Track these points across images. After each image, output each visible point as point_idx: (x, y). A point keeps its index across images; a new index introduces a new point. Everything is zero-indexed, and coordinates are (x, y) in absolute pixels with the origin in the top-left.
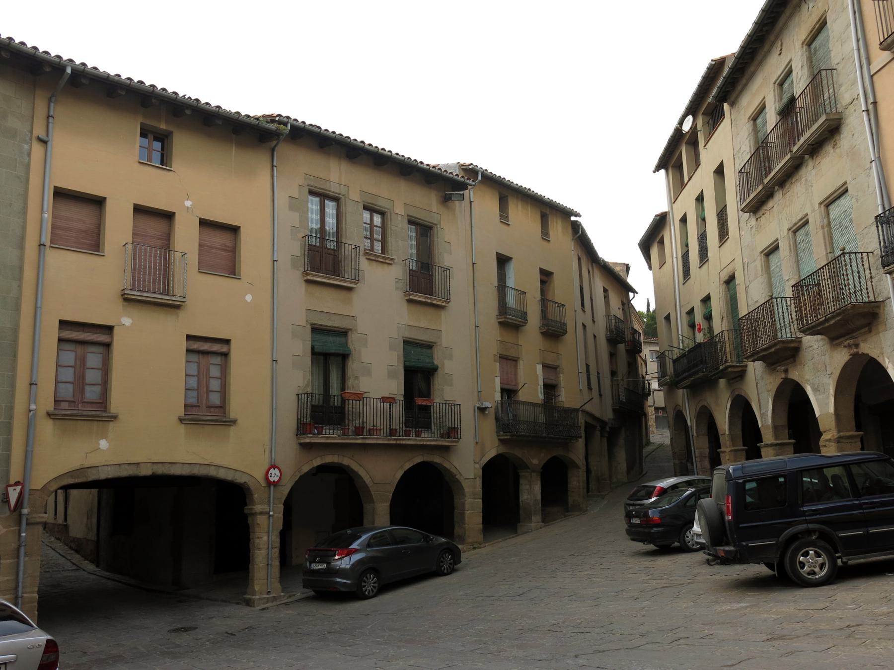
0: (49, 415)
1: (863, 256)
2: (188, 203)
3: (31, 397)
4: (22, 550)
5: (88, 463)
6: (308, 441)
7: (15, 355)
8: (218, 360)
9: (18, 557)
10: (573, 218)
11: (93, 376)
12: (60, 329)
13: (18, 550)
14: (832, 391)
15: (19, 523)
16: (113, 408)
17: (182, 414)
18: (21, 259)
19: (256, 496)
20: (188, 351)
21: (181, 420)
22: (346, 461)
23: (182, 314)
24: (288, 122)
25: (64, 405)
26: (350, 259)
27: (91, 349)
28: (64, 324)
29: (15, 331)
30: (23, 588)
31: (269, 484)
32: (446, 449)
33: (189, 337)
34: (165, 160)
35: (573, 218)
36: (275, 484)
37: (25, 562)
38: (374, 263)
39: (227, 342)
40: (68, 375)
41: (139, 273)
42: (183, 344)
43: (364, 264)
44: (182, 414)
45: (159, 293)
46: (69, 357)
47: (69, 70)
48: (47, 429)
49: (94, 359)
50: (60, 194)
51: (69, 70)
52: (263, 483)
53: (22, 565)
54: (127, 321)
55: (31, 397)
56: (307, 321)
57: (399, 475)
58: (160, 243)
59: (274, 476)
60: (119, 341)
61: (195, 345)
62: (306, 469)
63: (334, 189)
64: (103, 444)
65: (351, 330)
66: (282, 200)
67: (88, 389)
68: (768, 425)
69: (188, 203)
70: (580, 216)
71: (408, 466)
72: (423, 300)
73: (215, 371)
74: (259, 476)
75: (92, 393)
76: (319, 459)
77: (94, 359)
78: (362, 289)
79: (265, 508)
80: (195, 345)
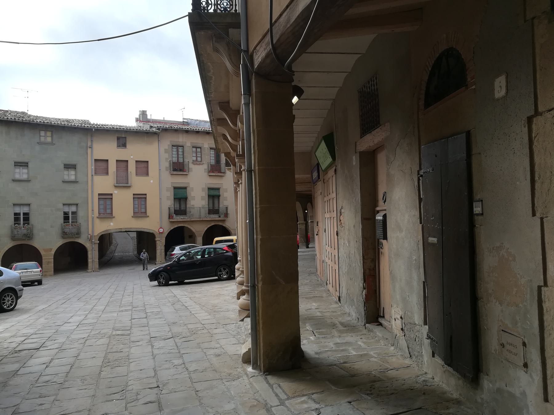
0: (97, 217)
1: (544, 110)
2: (132, 157)
3: (93, 214)
4: (93, 249)
5: (108, 229)
6: (171, 221)
7: (88, 204)
8: (144, 200)
9: (92, 251)
11: (108, 207)
12: (99, 195)
13: (92, 250)
15: (92, 244)
16: (114, 215)
17: (133, 216)
18: (88, 179)
19: (156, 236)
21: (132, 217)
22: (186, 225)
23: (131, 188)
24: (160, 128)
25: (102, 215)
26: (187, 165)
27: (108, 200)
28: (99, 194)
29: (88, 198)
30: (94, 258)
31: (160, 233)
32: (224, 221)
33: (134, 194)
34: (124, 145)
36: (162, 233)
37: (94, 253)
38: (196, 165)
40: (102, 207)
41: (119, 178)
42: (132, 196)
43: (191, 166)
44: (133, 216)
45: (118, 184)
46: (102, 202)
47: (94, 130)
48: (97, 221)
49: (108, 202)
50: (95, 160)
51: (94, 130)
52: (158, 233)
53: (93, 253)
54: (116, 192)
55: (93, 214)
56: (171, 186)
57: (206, 229)
58: (125, 169)
59: (161, 230)
60: (114, 197)
61: (101, 197)
62: (172, 228)
63: (181, 144)
64: (112, 224)
65: (187, 187)
66: (162, 150)
67: (107, 210)
69: (132, 157)
71: (209, 226)
72: (215, 175)
73: (143, 203)
74: (157, 231)
75: (109, 211)
76: (176, 225)
77: (108, 202)
78: (191, 174)
79: (159, 239)
80: (101, 197)
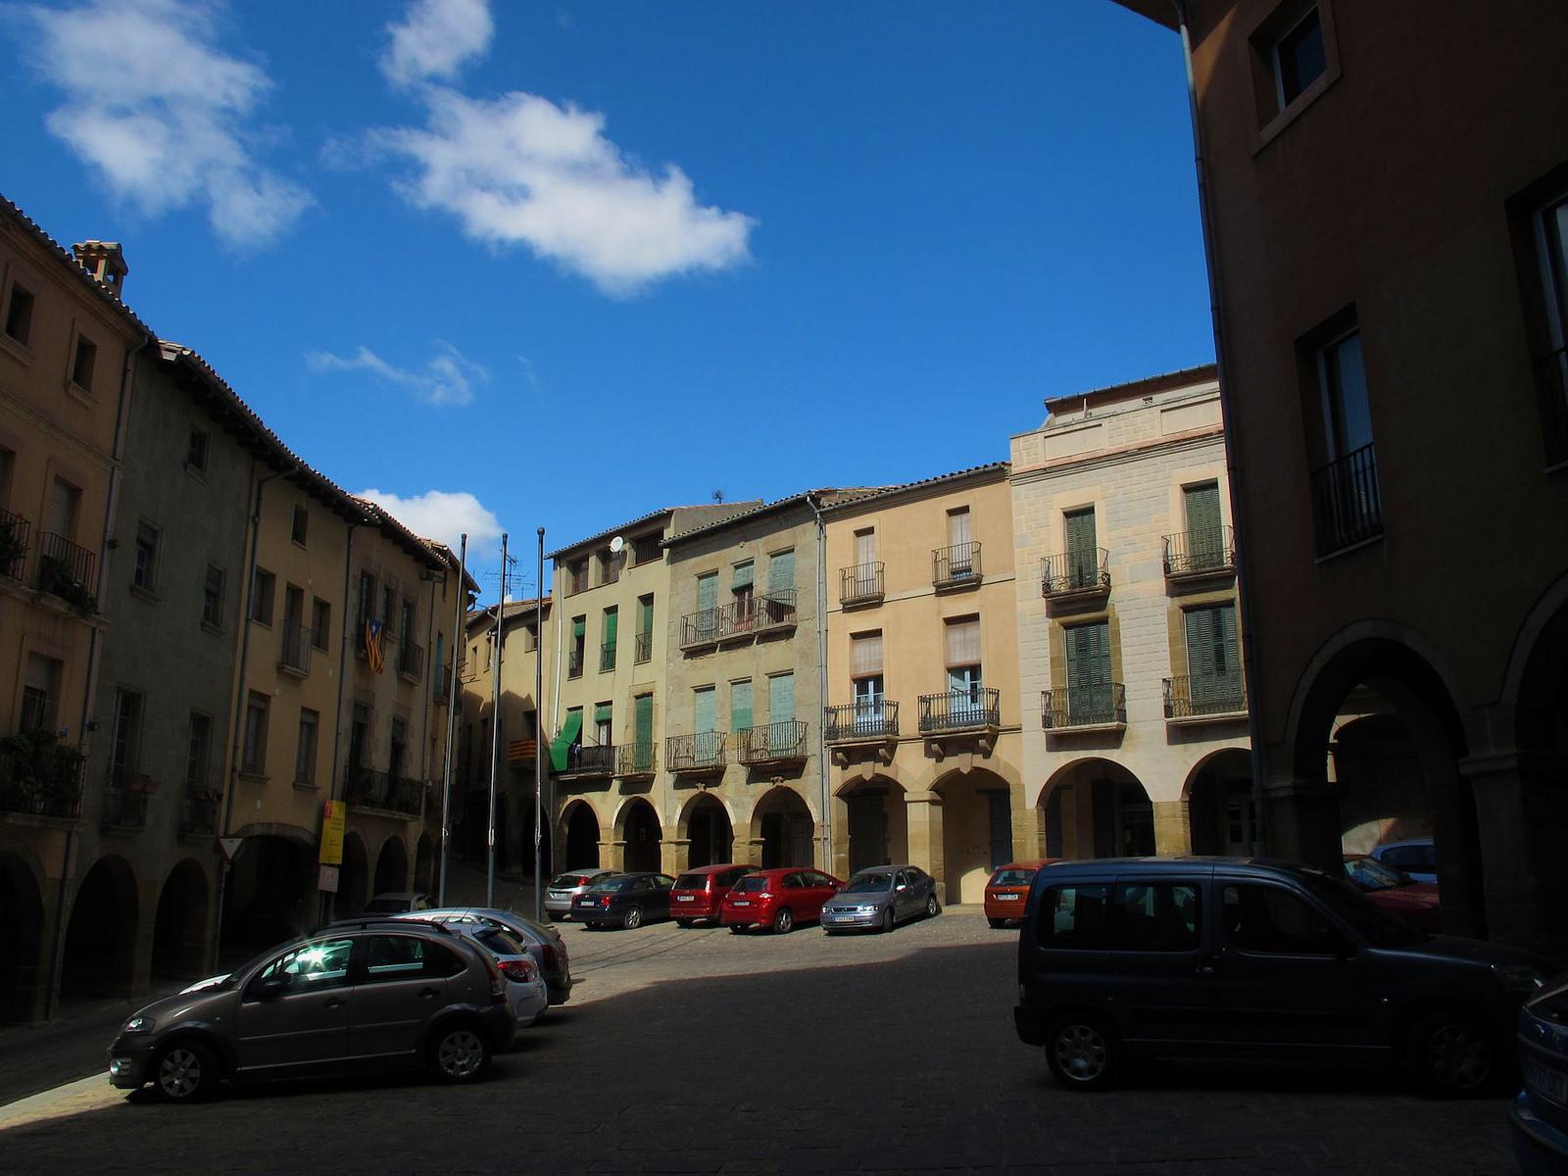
10: (470, 592)
14: (752, 808)
20: (302, 723)
33: (304, 709)
35: (470, 592)
39: (316, 714)
42: (298, 717)
68: (672, 827)
70: (479, 592)
